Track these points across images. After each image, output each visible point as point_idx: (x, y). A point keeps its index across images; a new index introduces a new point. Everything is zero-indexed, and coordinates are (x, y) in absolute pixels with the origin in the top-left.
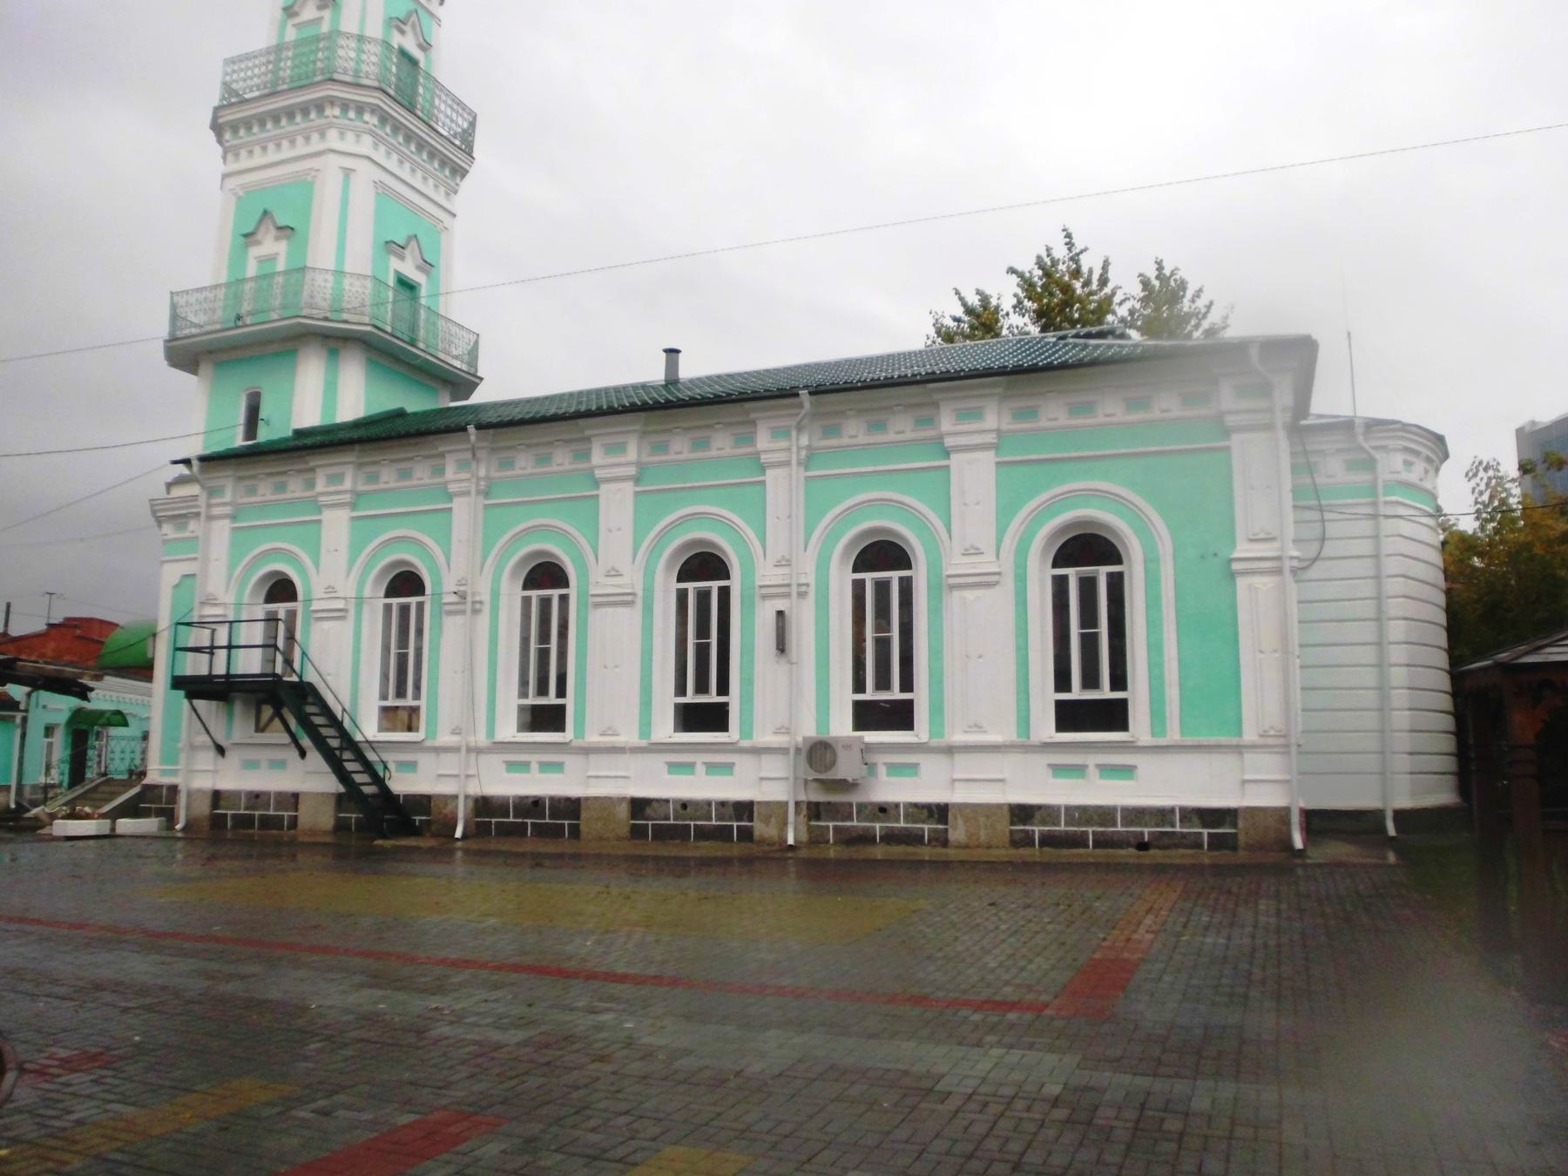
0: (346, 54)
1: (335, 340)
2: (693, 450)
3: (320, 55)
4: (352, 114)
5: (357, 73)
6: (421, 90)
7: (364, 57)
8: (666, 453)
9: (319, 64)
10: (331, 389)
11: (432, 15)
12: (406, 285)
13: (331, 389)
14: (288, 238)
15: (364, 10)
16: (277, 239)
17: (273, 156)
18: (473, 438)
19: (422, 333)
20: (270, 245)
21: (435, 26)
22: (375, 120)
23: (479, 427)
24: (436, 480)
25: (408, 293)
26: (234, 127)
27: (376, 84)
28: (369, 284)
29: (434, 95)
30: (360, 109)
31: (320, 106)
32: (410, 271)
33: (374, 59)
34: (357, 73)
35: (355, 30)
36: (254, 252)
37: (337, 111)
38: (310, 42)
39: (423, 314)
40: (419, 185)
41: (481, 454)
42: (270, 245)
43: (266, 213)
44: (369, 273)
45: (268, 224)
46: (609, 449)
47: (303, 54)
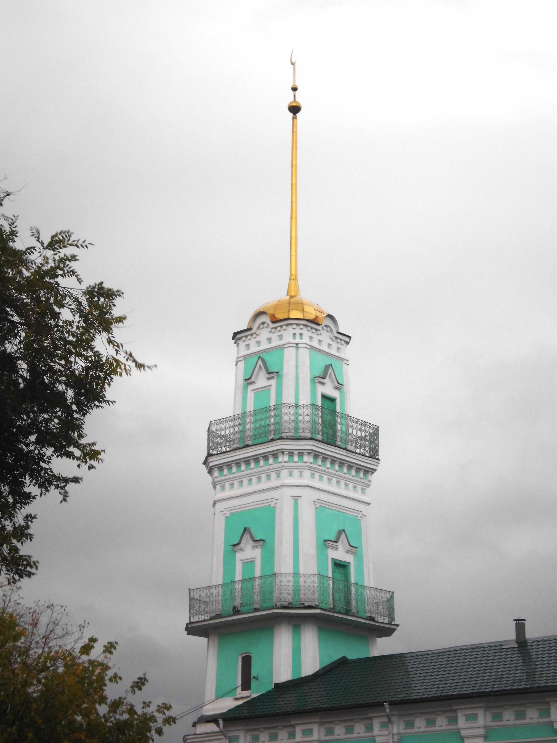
0: (288, 415)
1: (296, 616)
2: (517, 719)
3: (272, 420)
4: (296, 458)
5: (296, 429)
6: (339, 427)
7: (301, 418)
8: (501, 720)
9: (272, 427)
10: (297, 652)
11: (341, 359)
12: (340, 566)
13: (297, 652)
14: (261, 546)
15: (297, 378)
16: (254, 547)
17: (246, 489)
18: (388, 710)
19: (354, 603)
20: (249, 552)
21: (345, 366)
22: (311, 459)
23: (391, 704)
24: (367, 734)
25: (342, 570)
26: (220, 468)
27: (309, 435)
28: (316, 579)
29: (348, 426)
30: (301, 454)
31: (275, 455)
32: (341, 554)
33: (307, 418)
34: (296, 429)
35: (292, 401)
36: (240, 556)
37: (286, 458)
38: (262, 411)
39: (353, 590)
40: (343, 492)
41: (394, 719)
42: (249, 552)
43: (245, 529)
44: (316, 572)
45: (247, 536)
46: (469, 718)
47: (261, 419)
